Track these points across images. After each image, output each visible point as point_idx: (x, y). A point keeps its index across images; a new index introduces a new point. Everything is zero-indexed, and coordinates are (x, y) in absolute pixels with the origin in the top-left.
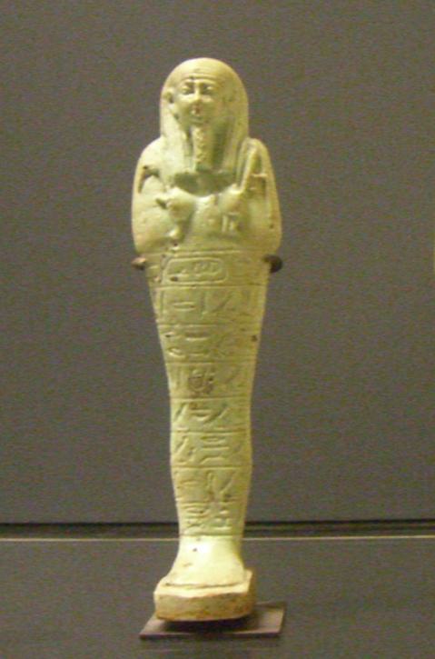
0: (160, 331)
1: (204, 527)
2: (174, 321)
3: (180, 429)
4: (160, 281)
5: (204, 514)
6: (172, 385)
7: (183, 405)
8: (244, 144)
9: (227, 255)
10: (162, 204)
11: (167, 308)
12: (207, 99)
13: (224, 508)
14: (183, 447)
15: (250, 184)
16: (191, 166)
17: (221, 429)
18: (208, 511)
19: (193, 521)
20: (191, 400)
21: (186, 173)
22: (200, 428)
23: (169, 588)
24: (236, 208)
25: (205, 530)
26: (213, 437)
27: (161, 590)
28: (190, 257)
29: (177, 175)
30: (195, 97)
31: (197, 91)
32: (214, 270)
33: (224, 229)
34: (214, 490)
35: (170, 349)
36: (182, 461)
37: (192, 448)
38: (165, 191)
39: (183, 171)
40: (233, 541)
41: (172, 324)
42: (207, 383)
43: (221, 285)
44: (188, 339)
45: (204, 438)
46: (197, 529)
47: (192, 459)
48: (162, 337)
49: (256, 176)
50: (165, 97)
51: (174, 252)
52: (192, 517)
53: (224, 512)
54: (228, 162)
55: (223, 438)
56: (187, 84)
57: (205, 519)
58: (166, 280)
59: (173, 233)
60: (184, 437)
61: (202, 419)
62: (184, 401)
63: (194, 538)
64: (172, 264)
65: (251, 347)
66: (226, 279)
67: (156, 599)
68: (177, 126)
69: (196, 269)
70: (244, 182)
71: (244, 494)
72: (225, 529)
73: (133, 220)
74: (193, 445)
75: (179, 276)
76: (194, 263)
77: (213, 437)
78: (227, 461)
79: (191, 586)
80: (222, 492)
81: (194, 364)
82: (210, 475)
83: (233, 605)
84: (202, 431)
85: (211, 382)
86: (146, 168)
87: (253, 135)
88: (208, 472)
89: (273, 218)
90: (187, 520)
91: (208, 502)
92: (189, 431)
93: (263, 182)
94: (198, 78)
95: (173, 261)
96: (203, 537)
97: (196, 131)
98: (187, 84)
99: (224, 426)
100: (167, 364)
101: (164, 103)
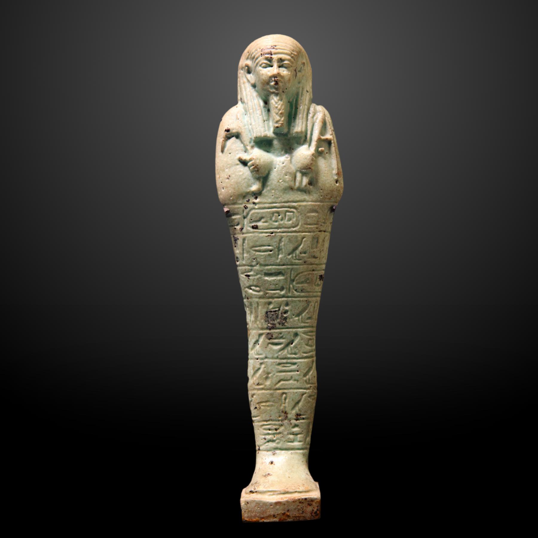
0: (240, 272)
1: (278, 443)
2: (254, 263)
3: (257, 357)
4: (242, 229)
5: (278, 431)
6: (250, 318)
7: (260, 335)
8: (312, 109)
9: (300, 206)
10: (244, 163)
11: (248, 252)
12: (284, 72)
13: (296, 426)
14: (260, 371)
15: (318, 147)
16: (269, 129)
17: (294, 356)
18: (282, 429)
19: (268, 437)
20: (268, 331)
21: (266, 136)
22: (276, 355)
23: (252, 494)
24: (306, 161)
25: (279, 446)
26: (287, 363)
27: (245, 496)
28: (269, 208)
29: (256, 138)
30: (274, 70)
31: (275, 65)
32: (290, 219)
33: (297, 184)
34: (288, 410)
35: (249, 287)
36: (258, 384)
37: (268, 373)
38: (246, 151)
39: (263, 134)
40: (304, 455)
41: (252, 266)
42: (282, 316)
43: (295, 232)
44: (266, 278)
46: (272, 445)
47: (268, 383)
49: (323, 138)
50: (242, 68)
51: (254, 203)
52: (269, 434)
53: (296, 429)
54: (298, 127)
55: (294, 364)
57: (279, 436)
58: (248, 228)
59: (255, 187)
60: (261, 364)
61: (279, 347)
62: (261, 332)
63: (270, 453)
64: (254, 213)
65: (318, 285)
66: (298, 227)
67: (242, 503)
68: (255, 94)
69: (274, 219)
70: (314, 143)
71: (310, 414)
72: (296, 444)
73: (217, 176)
74: (269, 370)
75: (260, 224)
76: (273, 213)
77: (287, 363)
78: (298, 384)
79: (274, 492)
80: (294, 412)
81: (270, 300)
82: (284, 395)
83: (310, 509)
84: (277, 358)
85: (285, 315)
86: (228, 131)
87: (316, 100)
88: (283, 393)
89: (338, 174)
90: (263, 437)
91: (282, 420)
92: (266, 358)
93: (329, 142)
94: (275, 54)
95: (253, 211)
96: (278, 452)
97: (274, 101)
98: (267, 59)
99: (295, 354)
101: (241, 73)
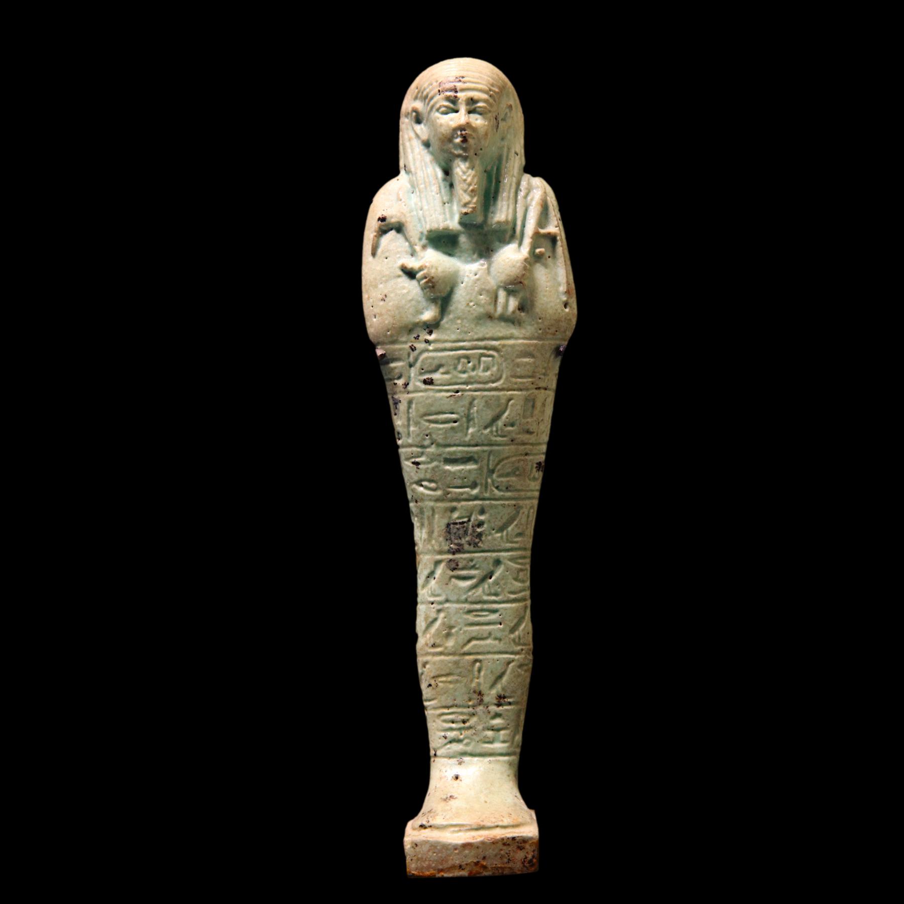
0: (402, 458)
1: (467, 744)
2: (427, 443)
3: (432, 599)
4: (406, 385)
5: (467, 724)
6: (420, 535)
7: (437, 563)
9: (504, 346)
10: (410, 274)
11: (417, 424)
12: (477, 121)
13: (497, 715)
14: (437, 624)
15: (534, 246)
16: (452, 217)
17: (493, 598)
18: (473, 721)
19: (451, 735)
21: (446, 229)
22: (463, 597)
23: (423, 831)
24: (515, 271)
25: (469, 749)
26: (482, 610)
27: (412, 834)
28: (452, 350)
29: (430, 231)
30: (460, 118)
31: (463, 109)
32: (487, 369)
33: (500, 309)
35: (419, 483)
36: (434, 646)
37: (451, 627)
38: (413, 254)
39: (441, 226)
40: (510, 764)
41: (423, 447)
42: (474, 531)
43: (496, 389)
44: (448, 467)
45: (469, 612)
46: (457, 747)
47: (450, 643)
48: (407, 465)
49: (542, 231)
51: (427, 341)
52: (451, 729)
53: (497, 722)
54: (501, 214)
55: (494, 611)
56: (448, 99)
57: (469, 732)
58: (416, 383)
59: (428, 315)
60: (439, 611)
61: (468, 583)
62: (439, 557)
63: (454, 761)
64: (426, 359)
66: (502, 382)
67: (407, 846)
68: (428, 158)
70: (527, 241)
72: (498, 746)
73: (365, 296)
75: (436, 376)
76: (459, 358)
77: (482, 610)
78: (500, 646)
79: (460, 827)
80: (494, 692)
81: (454, 504)
82: (478, 664)
83: (520, 855)
84: (466, 601)
85: (479, 530)
86: (382, 219)
87: (531, 168)
88: (476, 661)
89: (568, 292)
90: (443, 734)
91: (474, 706)
92: (447, 601)
93: (553, 239)
94: (462, 90)
95: (425, 355)
96: (467, 759)
97: (461, 169)
98: (448, 99)
99: (496, 594)
100: (412, 505)
101: (405, 123)
